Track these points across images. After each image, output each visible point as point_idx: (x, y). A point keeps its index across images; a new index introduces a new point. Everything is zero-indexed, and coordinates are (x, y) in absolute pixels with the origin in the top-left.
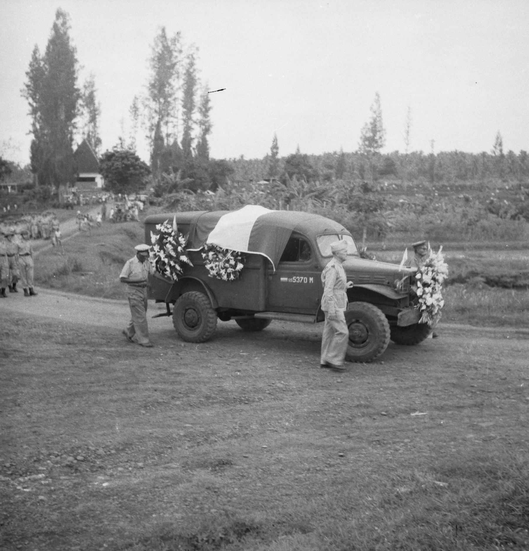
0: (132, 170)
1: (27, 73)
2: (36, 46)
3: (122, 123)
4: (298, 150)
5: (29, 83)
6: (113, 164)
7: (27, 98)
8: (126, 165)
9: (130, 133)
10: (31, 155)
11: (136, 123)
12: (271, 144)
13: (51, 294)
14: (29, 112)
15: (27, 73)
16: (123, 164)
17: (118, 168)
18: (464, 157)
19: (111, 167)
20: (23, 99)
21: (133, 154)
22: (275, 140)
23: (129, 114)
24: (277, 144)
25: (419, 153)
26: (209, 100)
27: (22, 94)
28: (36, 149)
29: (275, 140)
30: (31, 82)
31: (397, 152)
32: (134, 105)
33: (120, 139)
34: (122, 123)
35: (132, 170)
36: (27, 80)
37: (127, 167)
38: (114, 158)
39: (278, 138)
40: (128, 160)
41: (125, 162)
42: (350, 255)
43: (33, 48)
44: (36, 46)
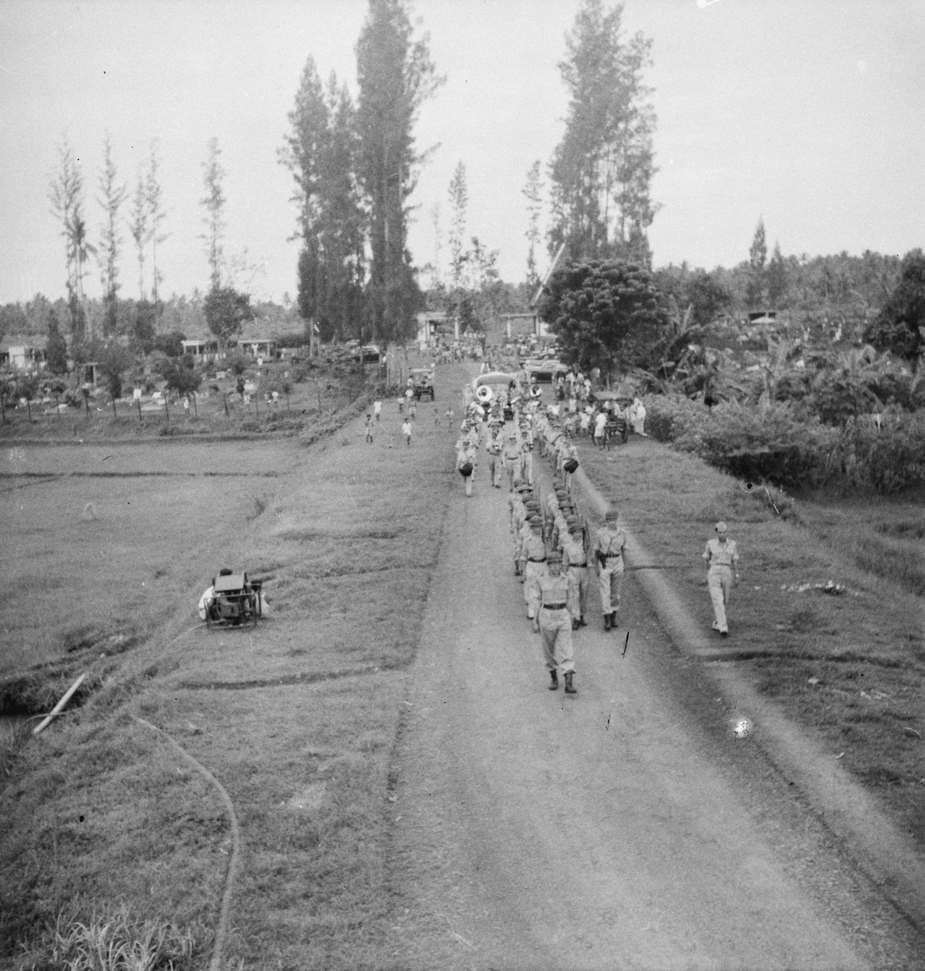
0: (638, 310)
1: (291, 115)
2: (310, 60)
5: (296, 136)
6: (590, 298)
7: (291, 168)
8: (623, 296)
9: (451, 232)
10: (299, 281)
11: (462, 214)
13: (59, 444)
15: (291, 115)
17: (605, 305)
18: (561, 273)
19: (585, 304)
20: (284, 168)
23: (449, 196)
24: (763, 240)
28: (309, 271)
30: (298, 131)
33: (476, 242)
34: (436, 215)
35: (638, 310)
36: (290, 130)
37: (626, 301)
38: (587, 281)
39: (766, 228)
41: (621, 289)
43: (303, 63)
44: (310, 60)
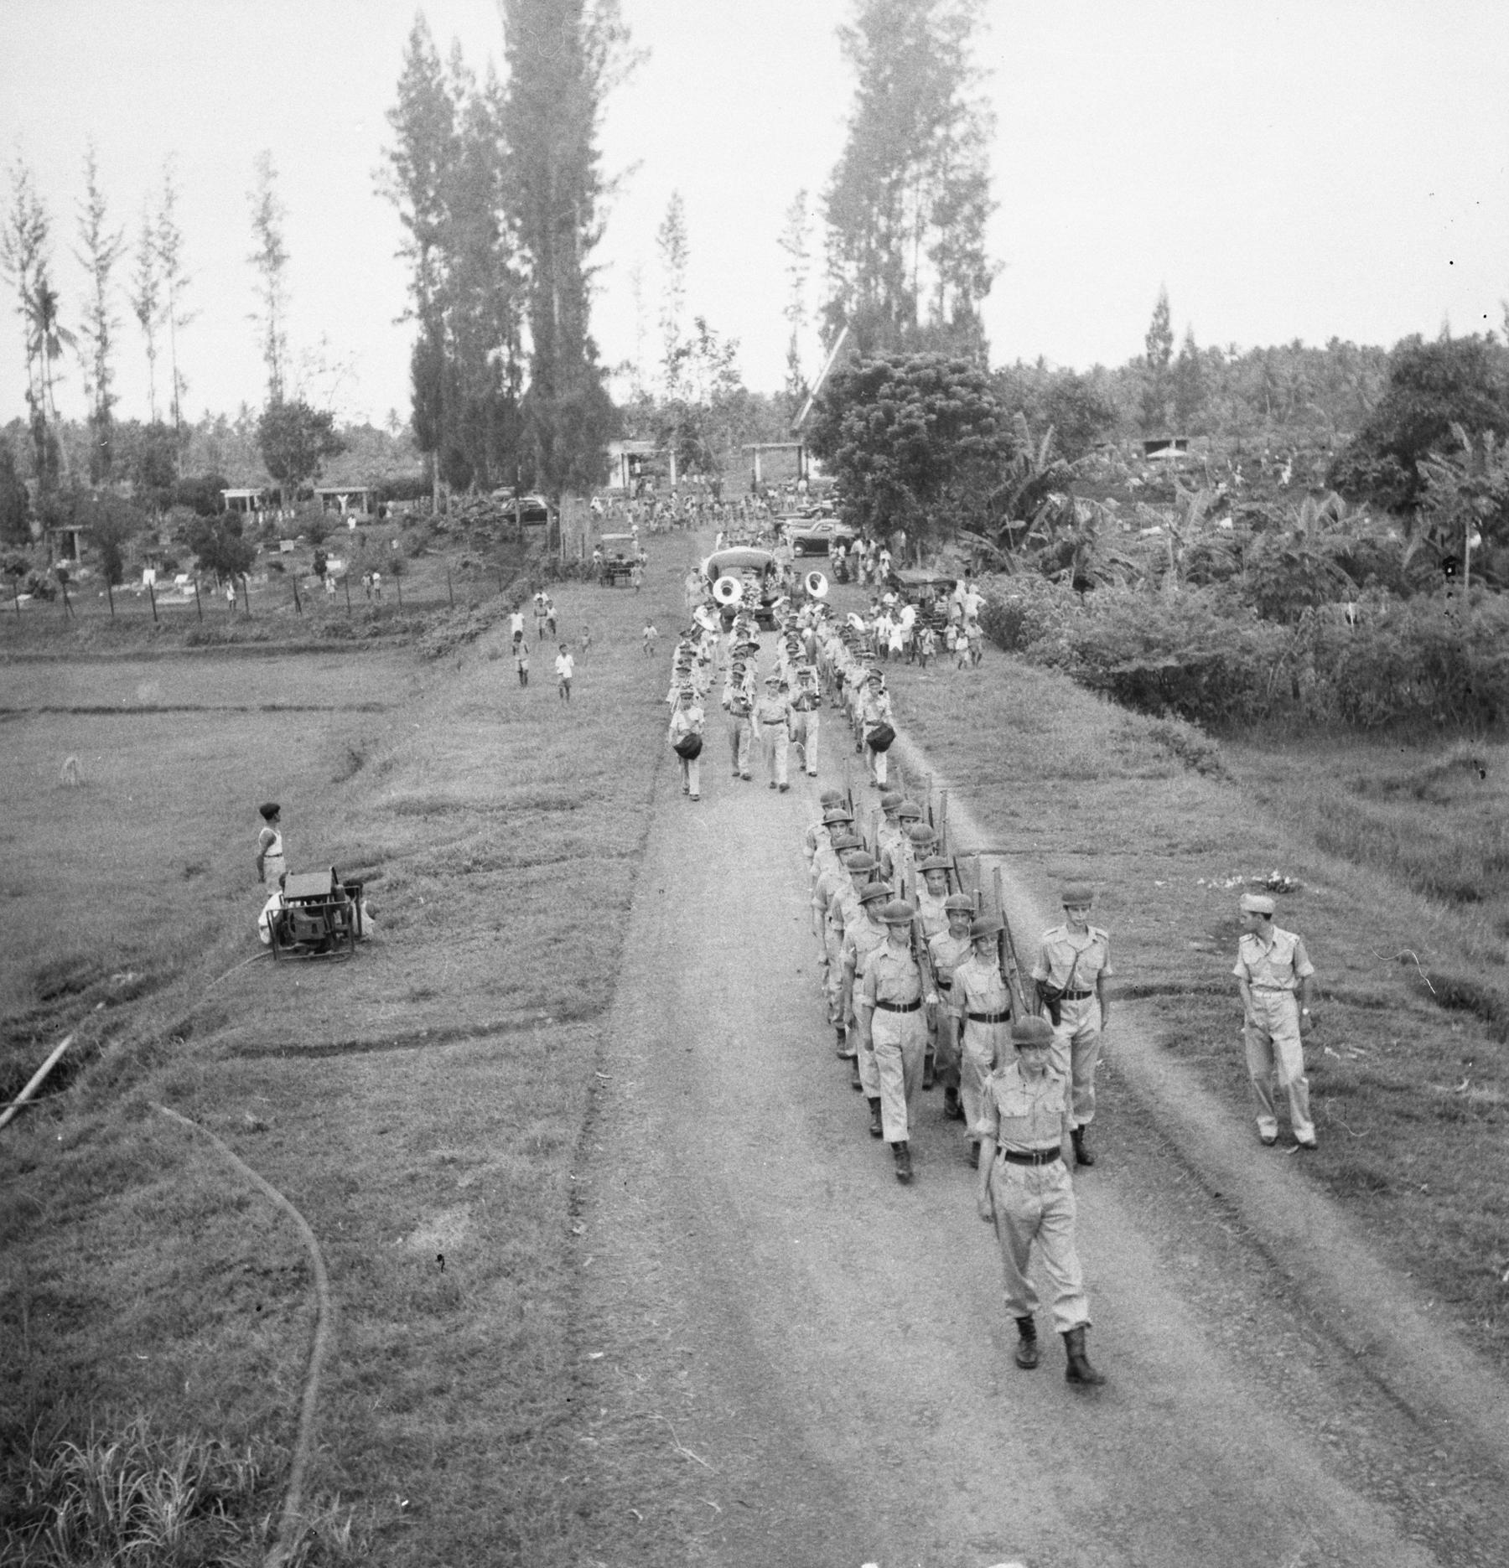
3: (637, 280)
4: (1446, 330)
6: (889, 417)
7: (395, 202)
8: (942, 413)
12: (1145, 324)
14: (823, 193)
16: (930, 408)
17: (912, 429)
19: (881, 426)
20: (384, 202)
21: (303, 410)
22: (1162, 309)
24: (1166, 322)
25: (1483, 337)
26: (54, 296)
27: (375, 185)
28: (431, 376)
29: (1162, 309)
31: (1418, 338)
32: (671, 219)
33: (701, 325)
34: (637, 280)
36: (393, 140)
37: (946, 423)
38: (885, 389)
40: (949, 396)
41: (940, 401)
42: (779, 722)
